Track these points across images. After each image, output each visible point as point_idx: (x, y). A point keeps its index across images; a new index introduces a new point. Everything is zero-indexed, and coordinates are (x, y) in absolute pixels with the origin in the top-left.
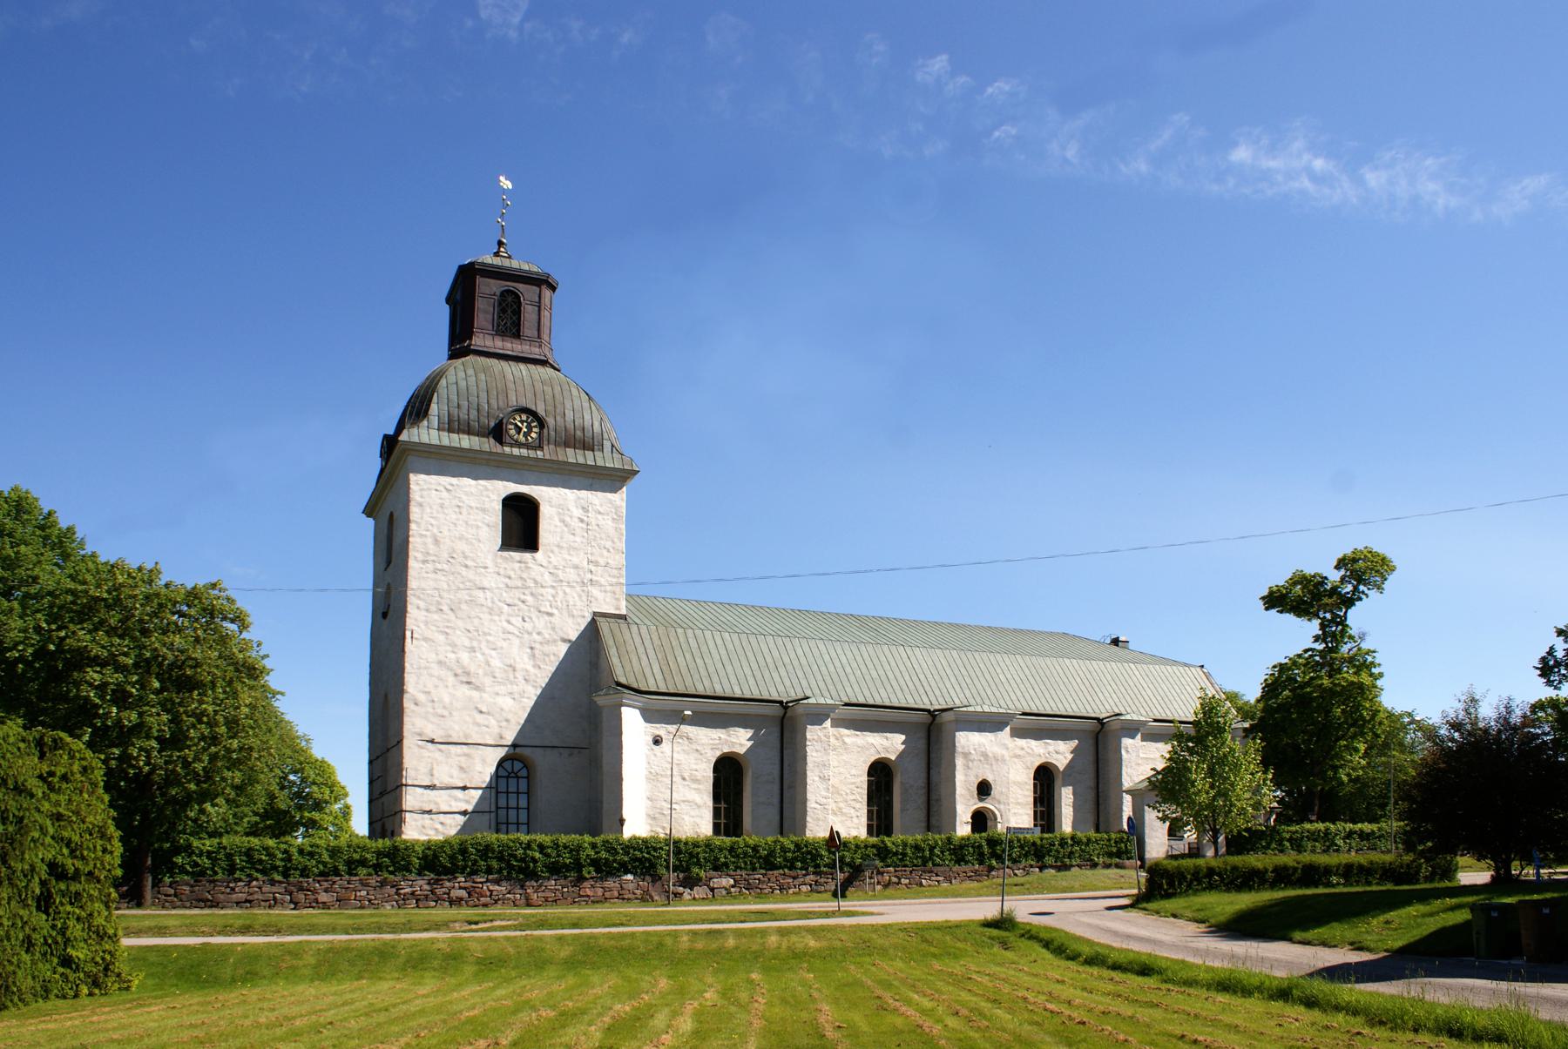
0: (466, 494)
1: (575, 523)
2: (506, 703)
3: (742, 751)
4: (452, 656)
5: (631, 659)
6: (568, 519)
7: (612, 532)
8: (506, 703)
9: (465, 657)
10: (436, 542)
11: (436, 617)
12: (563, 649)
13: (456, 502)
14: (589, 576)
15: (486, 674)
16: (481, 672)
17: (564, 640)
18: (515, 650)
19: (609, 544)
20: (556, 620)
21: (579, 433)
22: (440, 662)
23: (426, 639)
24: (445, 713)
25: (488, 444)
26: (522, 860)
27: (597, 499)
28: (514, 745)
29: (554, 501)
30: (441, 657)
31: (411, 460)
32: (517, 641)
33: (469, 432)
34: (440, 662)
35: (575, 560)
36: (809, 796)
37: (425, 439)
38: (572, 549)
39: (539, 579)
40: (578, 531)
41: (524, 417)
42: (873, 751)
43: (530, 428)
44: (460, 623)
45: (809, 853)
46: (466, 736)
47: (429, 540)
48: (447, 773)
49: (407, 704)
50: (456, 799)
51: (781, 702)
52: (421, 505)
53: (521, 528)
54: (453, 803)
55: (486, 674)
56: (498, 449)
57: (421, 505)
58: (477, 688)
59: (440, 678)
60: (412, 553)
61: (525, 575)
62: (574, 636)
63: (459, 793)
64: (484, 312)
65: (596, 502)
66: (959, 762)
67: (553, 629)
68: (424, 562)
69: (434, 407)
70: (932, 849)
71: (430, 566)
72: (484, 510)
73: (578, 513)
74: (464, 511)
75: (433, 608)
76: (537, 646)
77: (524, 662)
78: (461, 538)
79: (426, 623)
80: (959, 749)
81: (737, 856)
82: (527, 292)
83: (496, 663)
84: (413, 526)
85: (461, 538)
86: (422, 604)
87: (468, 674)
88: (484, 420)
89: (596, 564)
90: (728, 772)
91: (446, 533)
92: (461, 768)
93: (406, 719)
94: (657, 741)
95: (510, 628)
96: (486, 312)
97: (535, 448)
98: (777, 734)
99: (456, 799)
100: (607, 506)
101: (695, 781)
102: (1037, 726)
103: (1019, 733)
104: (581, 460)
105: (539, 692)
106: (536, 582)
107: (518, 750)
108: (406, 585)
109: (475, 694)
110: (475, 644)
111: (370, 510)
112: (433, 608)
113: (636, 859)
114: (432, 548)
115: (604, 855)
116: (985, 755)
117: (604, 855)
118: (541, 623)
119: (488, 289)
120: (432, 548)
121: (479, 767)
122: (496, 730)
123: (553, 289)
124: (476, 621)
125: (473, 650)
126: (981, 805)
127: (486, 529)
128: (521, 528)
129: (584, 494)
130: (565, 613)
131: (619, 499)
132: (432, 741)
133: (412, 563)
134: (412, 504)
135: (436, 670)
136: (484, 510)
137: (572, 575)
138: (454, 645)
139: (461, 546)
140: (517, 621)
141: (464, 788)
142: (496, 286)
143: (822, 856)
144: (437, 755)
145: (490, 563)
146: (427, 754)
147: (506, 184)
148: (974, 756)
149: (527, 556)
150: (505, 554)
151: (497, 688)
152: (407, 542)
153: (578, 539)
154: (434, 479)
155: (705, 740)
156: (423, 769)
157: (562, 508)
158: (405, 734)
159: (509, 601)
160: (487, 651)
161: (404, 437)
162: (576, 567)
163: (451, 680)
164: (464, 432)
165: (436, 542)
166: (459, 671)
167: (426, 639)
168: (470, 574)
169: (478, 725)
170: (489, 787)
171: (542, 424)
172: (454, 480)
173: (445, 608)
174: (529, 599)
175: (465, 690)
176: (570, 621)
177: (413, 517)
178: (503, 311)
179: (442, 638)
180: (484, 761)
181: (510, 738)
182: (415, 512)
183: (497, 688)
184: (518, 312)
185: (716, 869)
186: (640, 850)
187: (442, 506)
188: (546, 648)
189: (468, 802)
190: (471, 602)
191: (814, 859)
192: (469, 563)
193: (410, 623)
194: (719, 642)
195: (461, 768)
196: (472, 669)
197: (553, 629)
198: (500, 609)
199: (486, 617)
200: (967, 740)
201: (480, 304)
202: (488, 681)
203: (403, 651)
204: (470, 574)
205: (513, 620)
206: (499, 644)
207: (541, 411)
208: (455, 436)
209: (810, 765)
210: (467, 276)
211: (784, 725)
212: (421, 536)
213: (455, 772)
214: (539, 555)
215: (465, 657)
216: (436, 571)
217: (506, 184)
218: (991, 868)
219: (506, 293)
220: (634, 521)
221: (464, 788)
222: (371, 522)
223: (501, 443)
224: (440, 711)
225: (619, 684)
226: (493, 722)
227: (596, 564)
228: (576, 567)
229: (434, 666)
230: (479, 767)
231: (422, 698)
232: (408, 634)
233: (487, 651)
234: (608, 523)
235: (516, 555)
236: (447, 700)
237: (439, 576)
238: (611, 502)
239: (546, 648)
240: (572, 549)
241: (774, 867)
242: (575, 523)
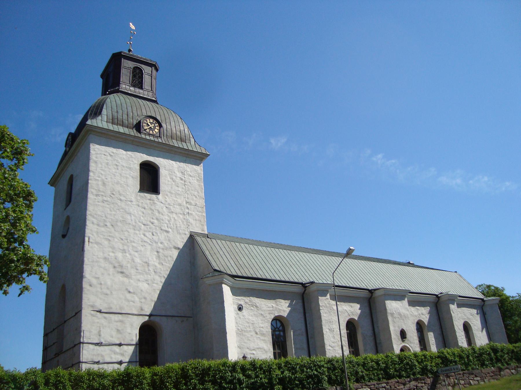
0: (121, 158)
1: (178, 180)
2: (144, 286)
3: (285, 315)
4: (112, 254)
5: (221, 256)
6: (174, 178)
7: (197, 187)
8: (144, 286)
9: (120, 255)
10: (104, 184)
11: (103, 229)
12: (175, 254)
13: (115, 162)
14: (187, 210)
15: (132, 267)
16: (129, 265)
17: (176, 248)
18: (148, 253)
19: (196, 193)
20: (170, 235)
21: (178, 133)
22: (105, 258)
23: (97, 243)
24: (108, 292)
25: (133, 132)
26: (231, 382)
27: (189, 168)
28: (150, 316)
29: (168, 169)
30: (106, 255)
31: (92, 136)
32: (149, 247)
33: (123, 126)
34: (105, 258)
35: (179, 201)
36: (325, 341)
37: (100, 125)
38: (177, 194)
39: (160, 210)
40: (180, 185)
41: (151, 121)
42: (346, 314)
43: (155, 127)
44: (117, 234)
45: (408, 364)
46: (121, 308)
47: (100, 183)
48: (109, 335)
49: (85, 285)
50: (115, 353)
51: (302, 284)
52: (96, 162)
53: (150, 179)
54: (113, 356)
55: (132, 267)
56: (139, 135)
57: (96, 162)
58: (127, 276)
59: (105, 269)
60: (90, 190)
61: (153, 208)
62: (181, 245)
63: (116, 349)
64: (125, 76)
65: (188, 170)
66: (390, 318)
67: (169, 240)
68: (97, 195)
69: (104, 112)
70: (468, 357)
71: (100, 198)
72: (130, 169)
73: (179, 175)
74: (119, 168)
75: (102, 224)
76: (161, 251)
77: (154, 261)
78: (118, 183)
79: (97, 233)
80: (389, 311)
81: (367, 370)
82: (146, 70)
83: (138, 260)
84: (91, 174)
85: (118, 183)
86: (95, 221)
87: (121, 266)
88: (131, 120)
89: (190, 204)
90: (279, 327)
91: (109, 179)
92: (118, 331)
93: (84, 296)
94: (240, 309)
95: (145, 239)
96: (127, 75)
97: (157, 137)
98: (301, 304)
99: (115, 353)
100: (194, 172)
101: (263, 334)
102: (416, 299)
103: (413, 303)
104: (181, 146)
105: (163, 280)
106: (159, 212)
107: (152, 318)
108: (86, 209)
109: (125, 279)
110: (126, 248)
111: (53, 182)
112: (102, 224)
113: (309, 377)
114: (101, 188)
115: (287, 373)
116: (400, 314)
117: (287, 373)
118: (162, 236)
119: (127, 65)
120: (101, 188)
121: (129, 330)
122: (139, 305)
123: (157, 70)
124: (126, 233)
125: (124, 251)
126: (403, 344)
127: (131, 179)
128: (150, 179)
129: (182, 165)
130: (175, 232)
131: (199, 169)
132: (100, 312)
133: (90, 195)
134: (91, 161)
135: (103, 264)
136: (130, 169)
137: (178, 209)
138: (113, 248)
139: (118, 188)
140: (149, 235)
141: (120, 345)
142: (131, 64)
143: (415, 365)
144: (103, 321)
145: (133, 199)
146: (97, 320)
147: (133, 27)
148: (395, 315)
149: (154, 196)
150: (142, 194)
151: (138, 277)
152: (87, 183)
153: (180, 189)
154: (103, 148)
155: (265, 308)
156: (95, 331)
157: (171, 172)
158: (84, 306)
159: (145, 222)
160: (133, 253)
161: (89, 122)
162: (180, 205)
163: (111, 270)
164: (120, 125)
165: (104, 184)
166: (116, 265)
167: (97, 243)
168: (123, 205)
169: (128, 301)
170: (136, 345)
171: (160, 126)
172: (114, 150)
173: (108, 224)
174: (155, 221)
175: (120, 278)
176: (178, 236)
177: (91, 168)
178: (134, 76)
179: (106, 243)
180: (132, 325)
181: (148, 309)
182: (92, 166)
183: (138, 277)
184: (141, 77)
185: (357, 381)
186: (310, 368)
187: (107, 164)
188: (166, 252)
189: (122, 355)
190: (124, 221)
191: (412, 369)
192: (122, 198)
193: (88, 232)
194: (259, 251)
195: (118, 331)
196: (124, 263)
197: (169, 240)
198: (140, 227)
199: (131, 231)
200: (392, 305)
201: (123, 71)
202: (133, 271)
203: (83, 250)
204: (123, 205)
205: (147, 234)
206: (140, 248)
207: (159, 118)
208: (115, 126)
209: (324, 322)
210: (116, 59)
211: (305, 296)
212: (96, 180)
213: (114, 333)
214: (160, 196)
215: (120, 255)
216: (103, 201)
217: (133, 27)
218: (500, 370)
219: (135, 68)
220: (208, 181)
221: (120, 345)
222: (53, 189)
223: (140, 132)
224: (105, 291)
225: (216, 270)
226: (137, 299)
227: (190, 204)
228: (180, 205)
229: (101, 260)
230: (129, 330)
231: (94, 281)
232: (86, 239)
233: (133, 253)
234: (194, 182)
235: (148, 196)
236: (109, 283)
237: (105, 204)
238: (195, 170)
239: (166, 252)
240: (177, 194)
241: (389, 377)
242: (178, 180)
